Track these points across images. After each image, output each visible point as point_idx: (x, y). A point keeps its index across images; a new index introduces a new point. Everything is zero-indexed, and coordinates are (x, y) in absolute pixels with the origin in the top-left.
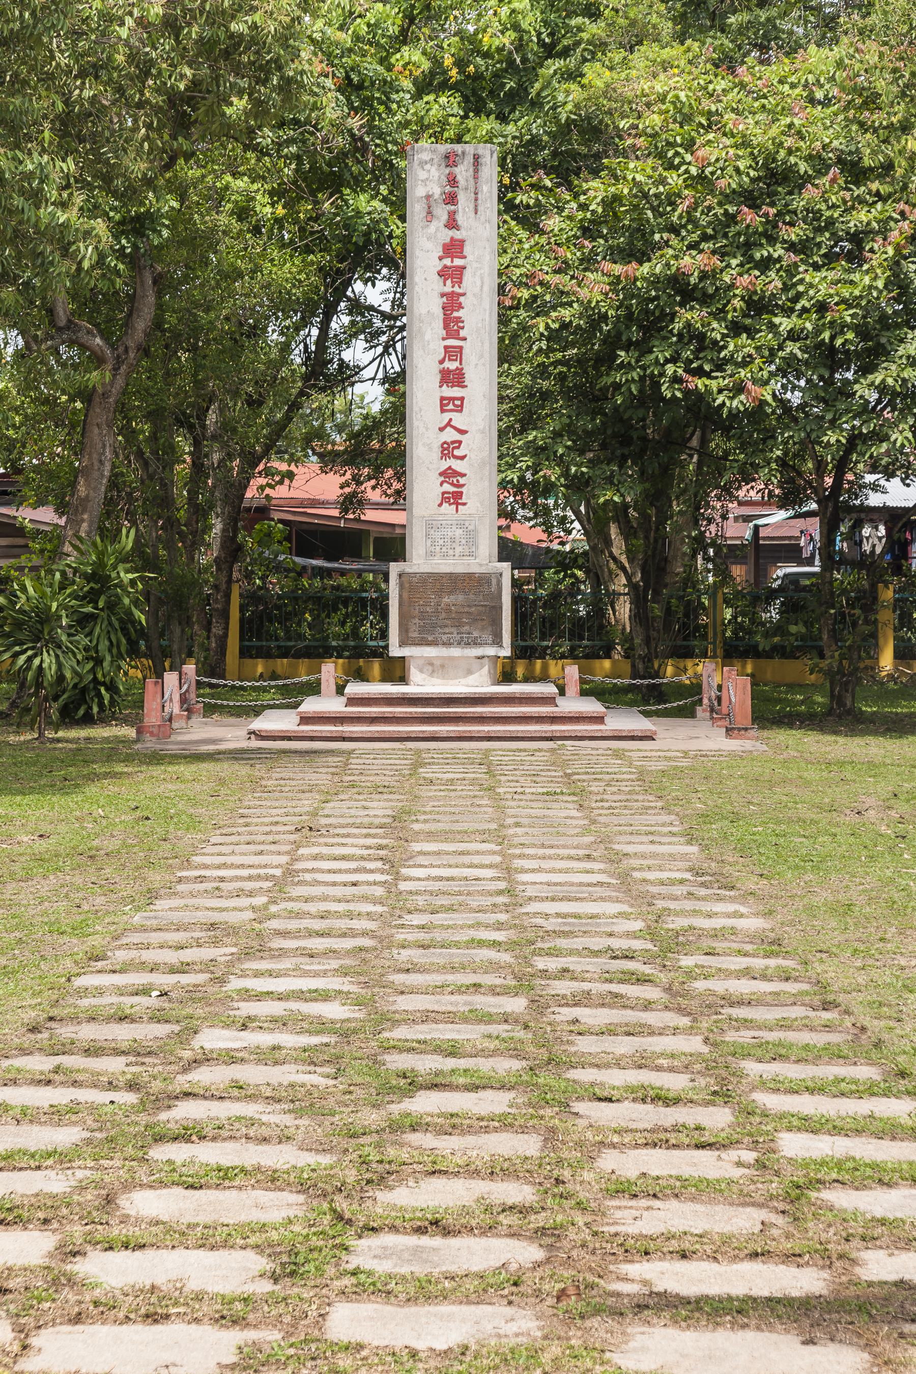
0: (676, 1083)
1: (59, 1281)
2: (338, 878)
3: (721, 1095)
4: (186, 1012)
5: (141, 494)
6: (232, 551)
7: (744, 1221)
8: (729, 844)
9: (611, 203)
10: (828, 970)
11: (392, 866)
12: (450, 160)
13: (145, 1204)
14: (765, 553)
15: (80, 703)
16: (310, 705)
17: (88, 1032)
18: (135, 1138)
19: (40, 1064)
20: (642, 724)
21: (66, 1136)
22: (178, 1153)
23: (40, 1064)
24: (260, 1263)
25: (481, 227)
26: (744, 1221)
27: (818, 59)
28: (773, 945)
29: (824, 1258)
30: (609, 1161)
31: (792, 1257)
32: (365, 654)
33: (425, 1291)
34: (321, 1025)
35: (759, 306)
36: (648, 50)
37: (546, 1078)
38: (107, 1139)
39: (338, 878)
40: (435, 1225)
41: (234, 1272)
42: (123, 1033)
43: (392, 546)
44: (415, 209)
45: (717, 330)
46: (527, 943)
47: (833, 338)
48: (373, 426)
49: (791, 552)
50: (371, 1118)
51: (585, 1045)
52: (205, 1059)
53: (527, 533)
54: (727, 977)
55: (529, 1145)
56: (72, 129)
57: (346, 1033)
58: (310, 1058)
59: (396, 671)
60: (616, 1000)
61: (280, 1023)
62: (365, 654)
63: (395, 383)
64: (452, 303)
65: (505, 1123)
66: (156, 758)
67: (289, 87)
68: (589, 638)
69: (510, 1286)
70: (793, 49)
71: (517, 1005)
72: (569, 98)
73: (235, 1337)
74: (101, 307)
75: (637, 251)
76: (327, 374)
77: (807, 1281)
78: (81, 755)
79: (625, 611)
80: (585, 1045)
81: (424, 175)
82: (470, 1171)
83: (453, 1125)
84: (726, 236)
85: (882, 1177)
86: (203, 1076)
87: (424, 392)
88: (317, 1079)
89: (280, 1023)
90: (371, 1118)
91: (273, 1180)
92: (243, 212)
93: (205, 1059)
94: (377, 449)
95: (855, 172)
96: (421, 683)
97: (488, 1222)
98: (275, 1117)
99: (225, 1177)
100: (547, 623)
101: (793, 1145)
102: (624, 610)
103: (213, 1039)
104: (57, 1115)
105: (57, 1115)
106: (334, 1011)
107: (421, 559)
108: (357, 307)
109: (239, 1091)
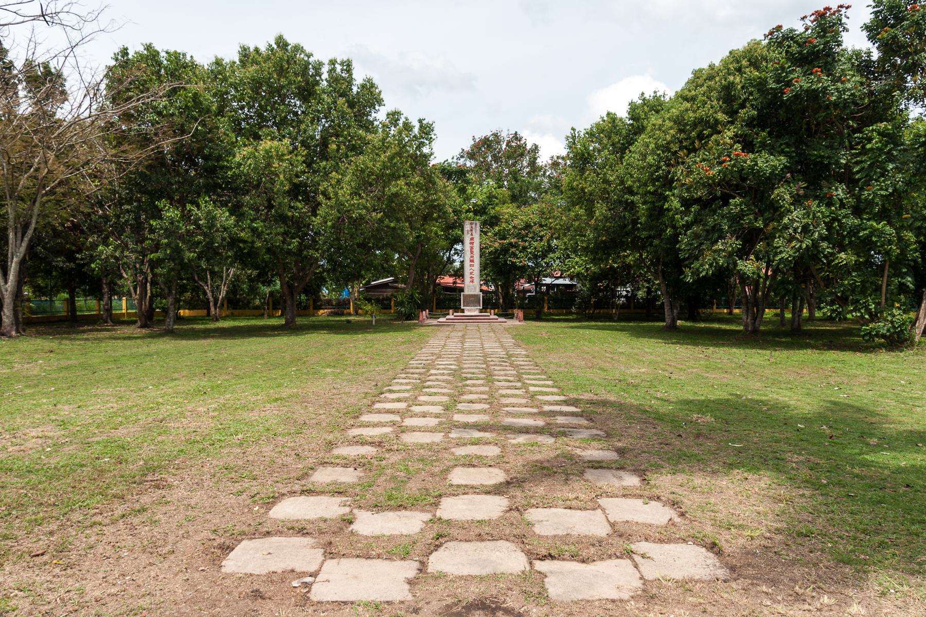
0: (512, 379)
1: (408, 411)
2: (453, 345)
3: (519, 381)
4: (428, 367)
5: (419, 282)
6: (434, 291)
7: (524, 401)
8: (519, 339)
9: (499, 231)
10: (537, 360)
11: (462, 344)
12: (471, 224)
13: (422, 398)
14: (525, 291)
15: (409, 317)
16: (448, 317)
17: (411, 371)
18: (420, 387)
19: (404, 376)
20: (504, 320)
21: (408, 387)
22: (427, 390)
23: (404, 376)
24: (441, 408)
25: (477, 236)
26: (524, 401)
27: (535, 206)
28: (527, 356)
29: (537, 407)
30: (500, 391)
31: (532, 407)
32: (457, 309)
33: (470, 412)
34: (451, 369)
35: (525, 248)
36: (506, 205)
37: (489, 378)
38: (415, 387)
39: (453, 345)
40: (471, 402)
41: (438, 409)
42: (418, 371)
43: (462, 290)
44: (465, 232)
45: (517, 252)
46: (485, 356)
47: (641, 255)
48: (458, 270)
49: (530, 291)
50: (460, 384)
51: (496, 372)
52: (431, 375)
53: (484, 288)
54: (520, 361)
55: (487, 389)
56: (408, 219)
57: (455, 370)
58: (449, 375)
59: (463, 311)
60: (501, 365)
61: (444, 369)
62: (457, 309)
63: (462, 262)
64: (472, 248)
65: (483, 385)
66: (422, 326)
67: (445, 213)
68: (495, 306)
69: (484, 412)
70: (530, 205)
71: (484, 366)
72: (492, 212)
73: (439, 420)
74: (412, 248)
75: (504, 238)
76: (450, 261)
77: (535, 410)
78: (415, 325)
79: (501, 302)
80: (496, 372)
81: (467, 227)
82: (477, 393)
83: (474, 385)
84: (519, 236)
85: (547, 394)
86: (431, 378)
87: (467, 264)
88: (450, 378)
89: (444, 369)
90: (460, 384)
91: (444, 394)
92: (436, 233)
93: (431, 375)
94: (459, 273)
95: (541, 226)
96: (467, 313)
97: (480, 401)
98: (444, 384)
99: (435, 394)
100: (488, 303)
101: (532, 389)
102: (501, 301)
103: (433, 372)
104: (407, 384)
105: (407, 384)
106: (453, 367)
107: (466, 292)
108: (456, 249)
109: (437, 380)
